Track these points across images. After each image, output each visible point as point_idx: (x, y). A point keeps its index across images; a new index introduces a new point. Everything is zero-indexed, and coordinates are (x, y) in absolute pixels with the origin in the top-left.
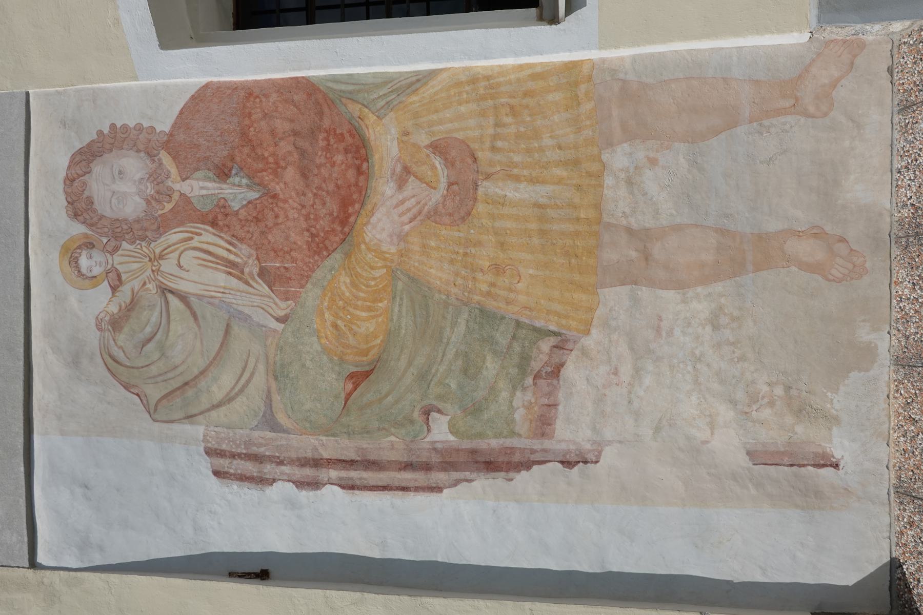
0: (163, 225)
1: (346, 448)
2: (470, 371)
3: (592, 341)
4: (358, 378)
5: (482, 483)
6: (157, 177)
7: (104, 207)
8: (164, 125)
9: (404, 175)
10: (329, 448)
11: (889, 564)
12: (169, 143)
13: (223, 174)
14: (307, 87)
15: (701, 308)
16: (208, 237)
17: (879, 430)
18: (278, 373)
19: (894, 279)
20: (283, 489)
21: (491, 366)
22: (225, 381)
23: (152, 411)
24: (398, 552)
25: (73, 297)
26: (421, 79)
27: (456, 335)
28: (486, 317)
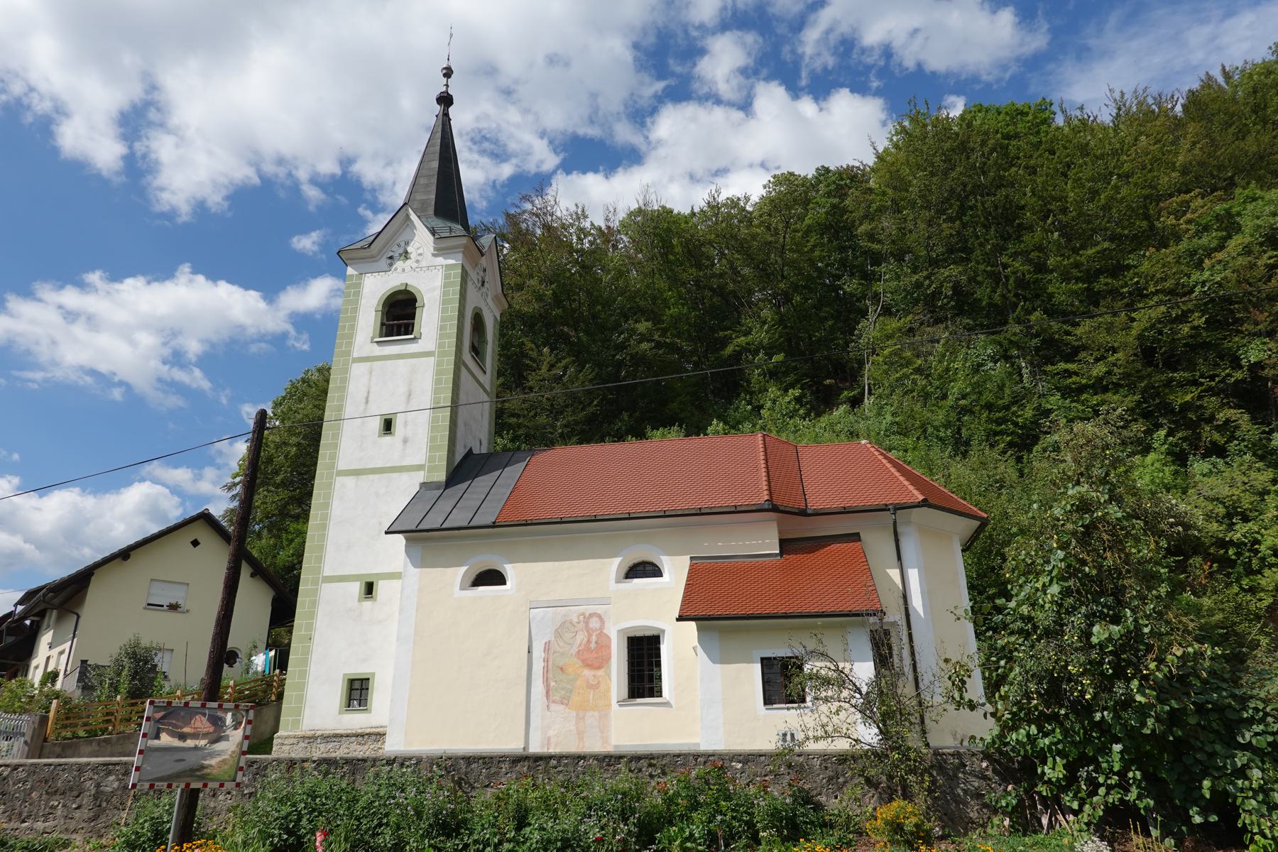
0: (588, 631)
1: (550, 667)
2: (562, 689)
3: (567, 710)
4: (561, 669)
5: (544, 691)
6: (596, 630)
7: (592, 620)
8: (605, 631)
9: (594, 676)
10: (550, 663)
11: (700, 622)
12: (601, 632)
13: (596, 643)
14: (609, 658)
15: (572, 728)
16: (586, 640)
17: (890, 191)
18: (562, 654)
19: (448, 235)
20: (543, 655)
21: (563, 692)
22: (562, 644)
23: (556, 630)
24: (533, 676)
25: (575, 615)
26: (610, 679)
27: (568, 686)
28: (571, 691)
